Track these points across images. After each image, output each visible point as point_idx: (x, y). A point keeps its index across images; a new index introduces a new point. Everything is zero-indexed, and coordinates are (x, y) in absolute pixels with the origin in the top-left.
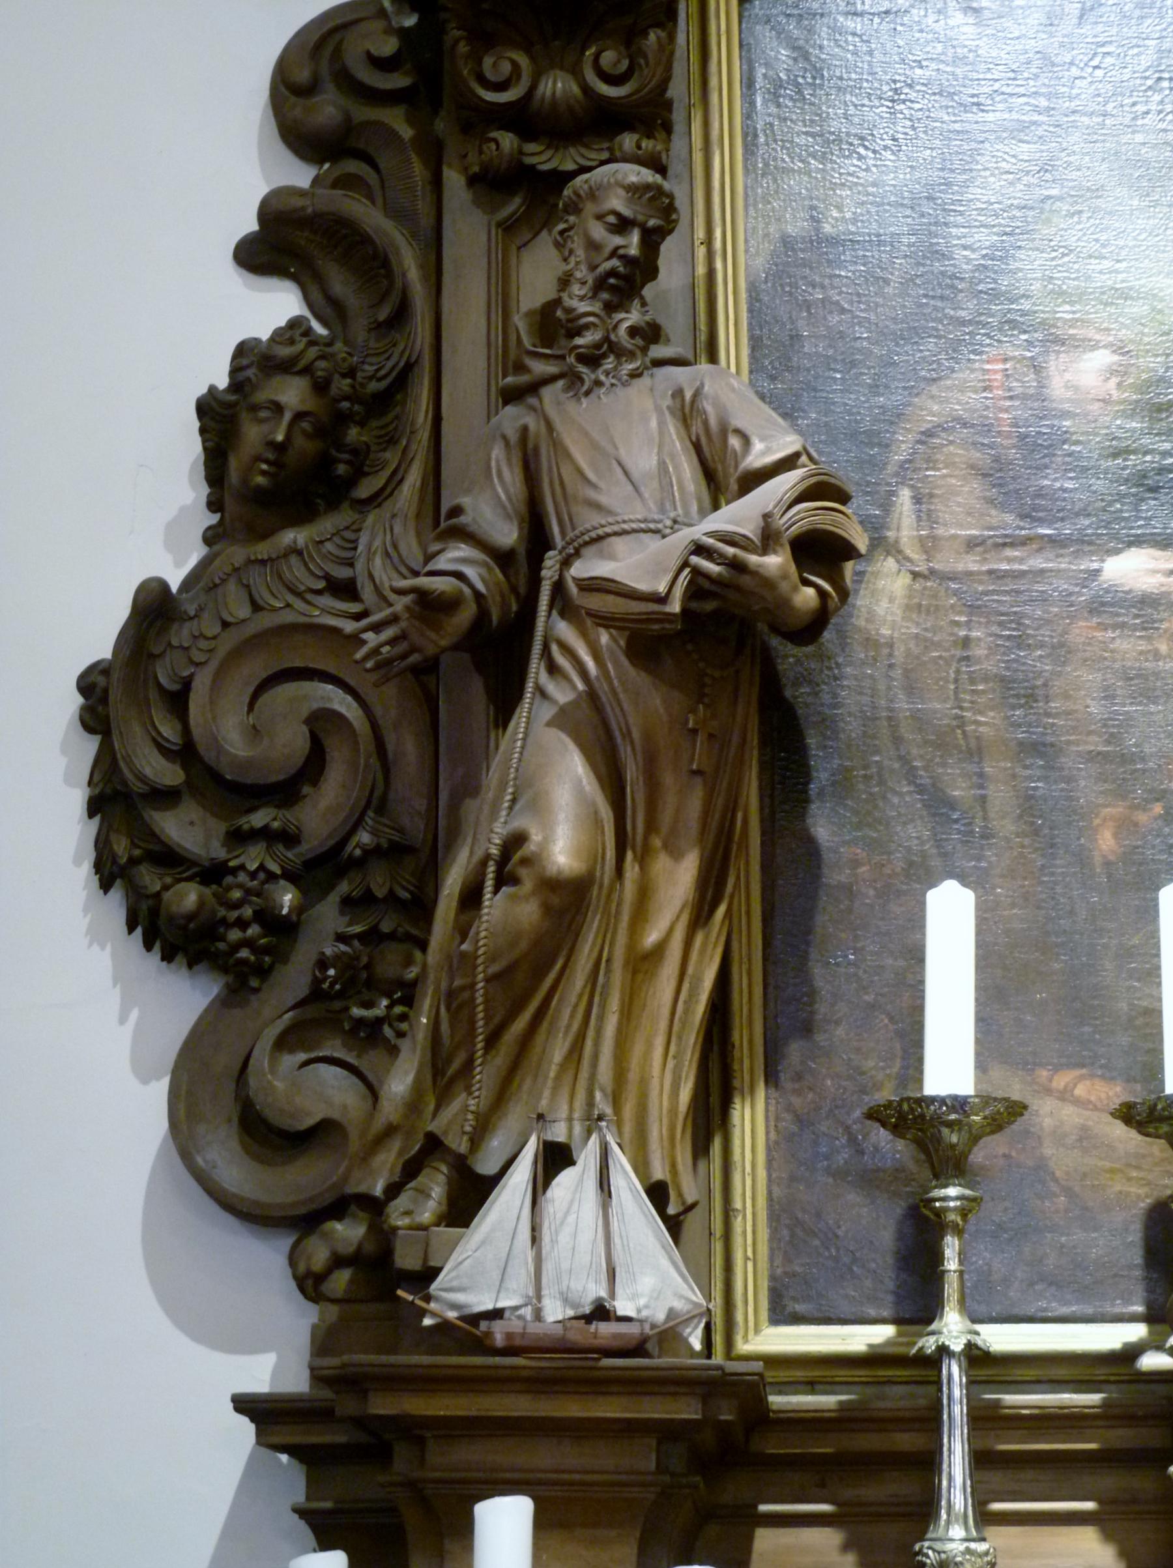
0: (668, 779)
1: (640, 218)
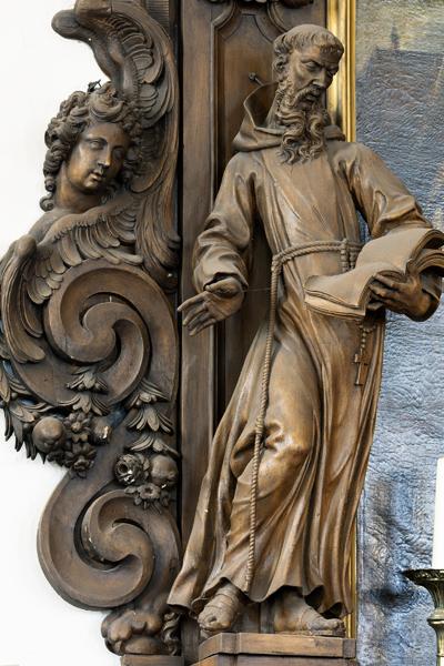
0: (343, 389)
1: (327, 64)
